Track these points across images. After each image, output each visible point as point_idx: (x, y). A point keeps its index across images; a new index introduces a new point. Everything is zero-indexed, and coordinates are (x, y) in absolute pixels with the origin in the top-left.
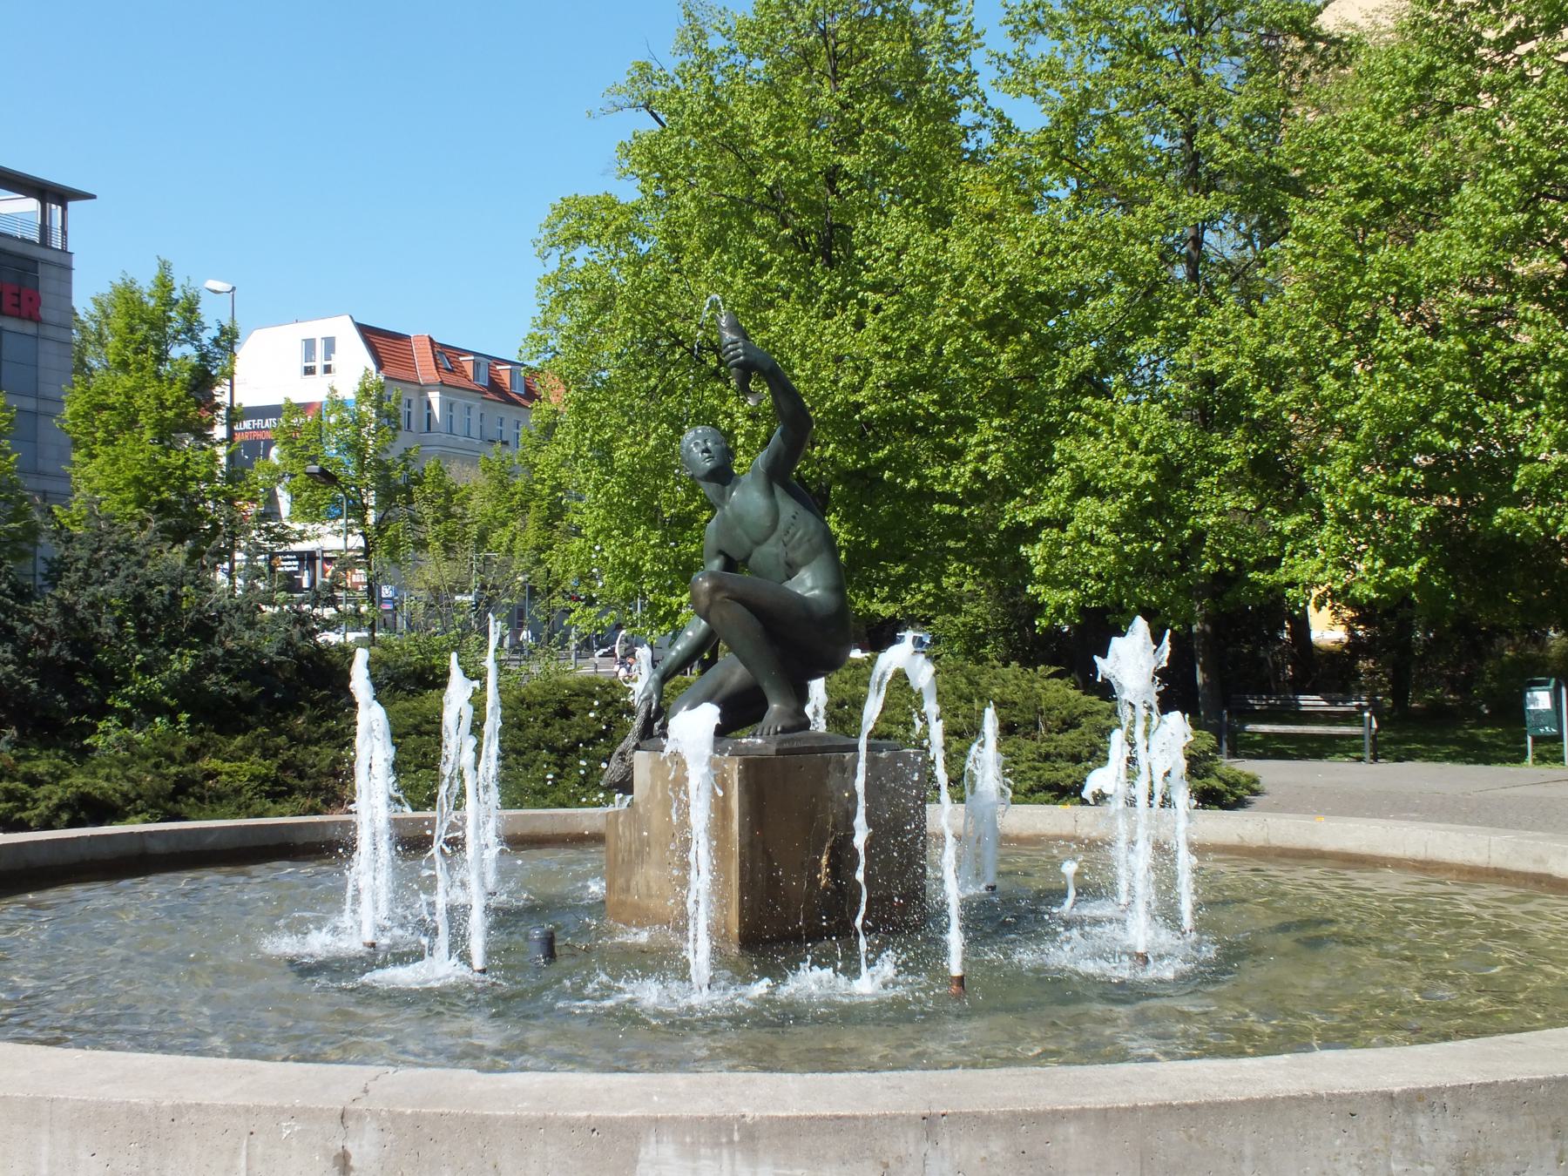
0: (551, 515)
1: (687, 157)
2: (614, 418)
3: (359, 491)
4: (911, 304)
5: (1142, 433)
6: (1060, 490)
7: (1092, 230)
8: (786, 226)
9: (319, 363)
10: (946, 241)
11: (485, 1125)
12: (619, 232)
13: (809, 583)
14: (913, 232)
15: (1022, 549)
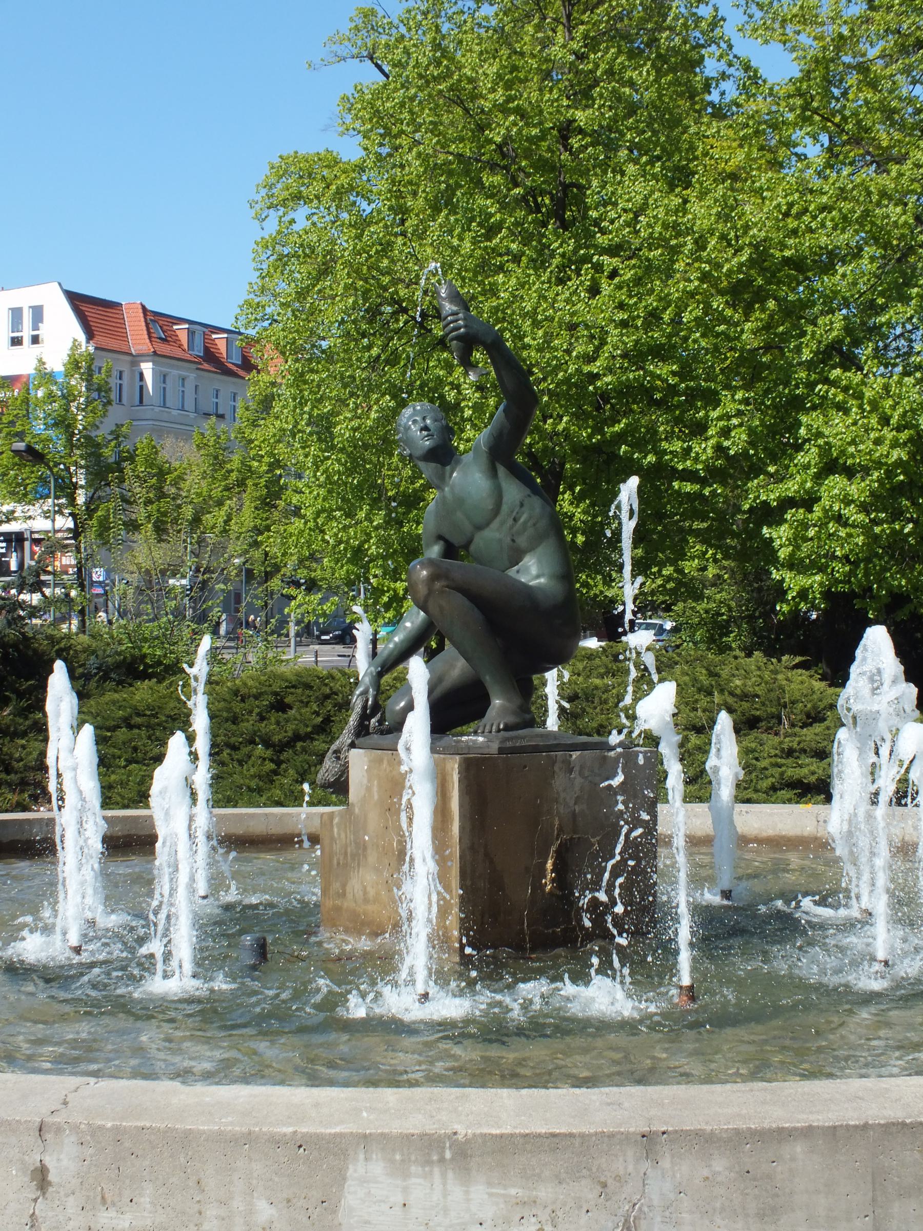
0: (269, 495)
1: (411, 112)
2: (335, 390)
3: (67, 469)
4: (649, 268)
5: (893, 408)
6: (807, 467)
7: (842, 190)
8: (516, 185)
9: (26, 333)
10: (686, 201)
11: (187, 1139)
12: (339, 194)
13: (534, 571)
14: (652, 192)
15: (765, 530)
